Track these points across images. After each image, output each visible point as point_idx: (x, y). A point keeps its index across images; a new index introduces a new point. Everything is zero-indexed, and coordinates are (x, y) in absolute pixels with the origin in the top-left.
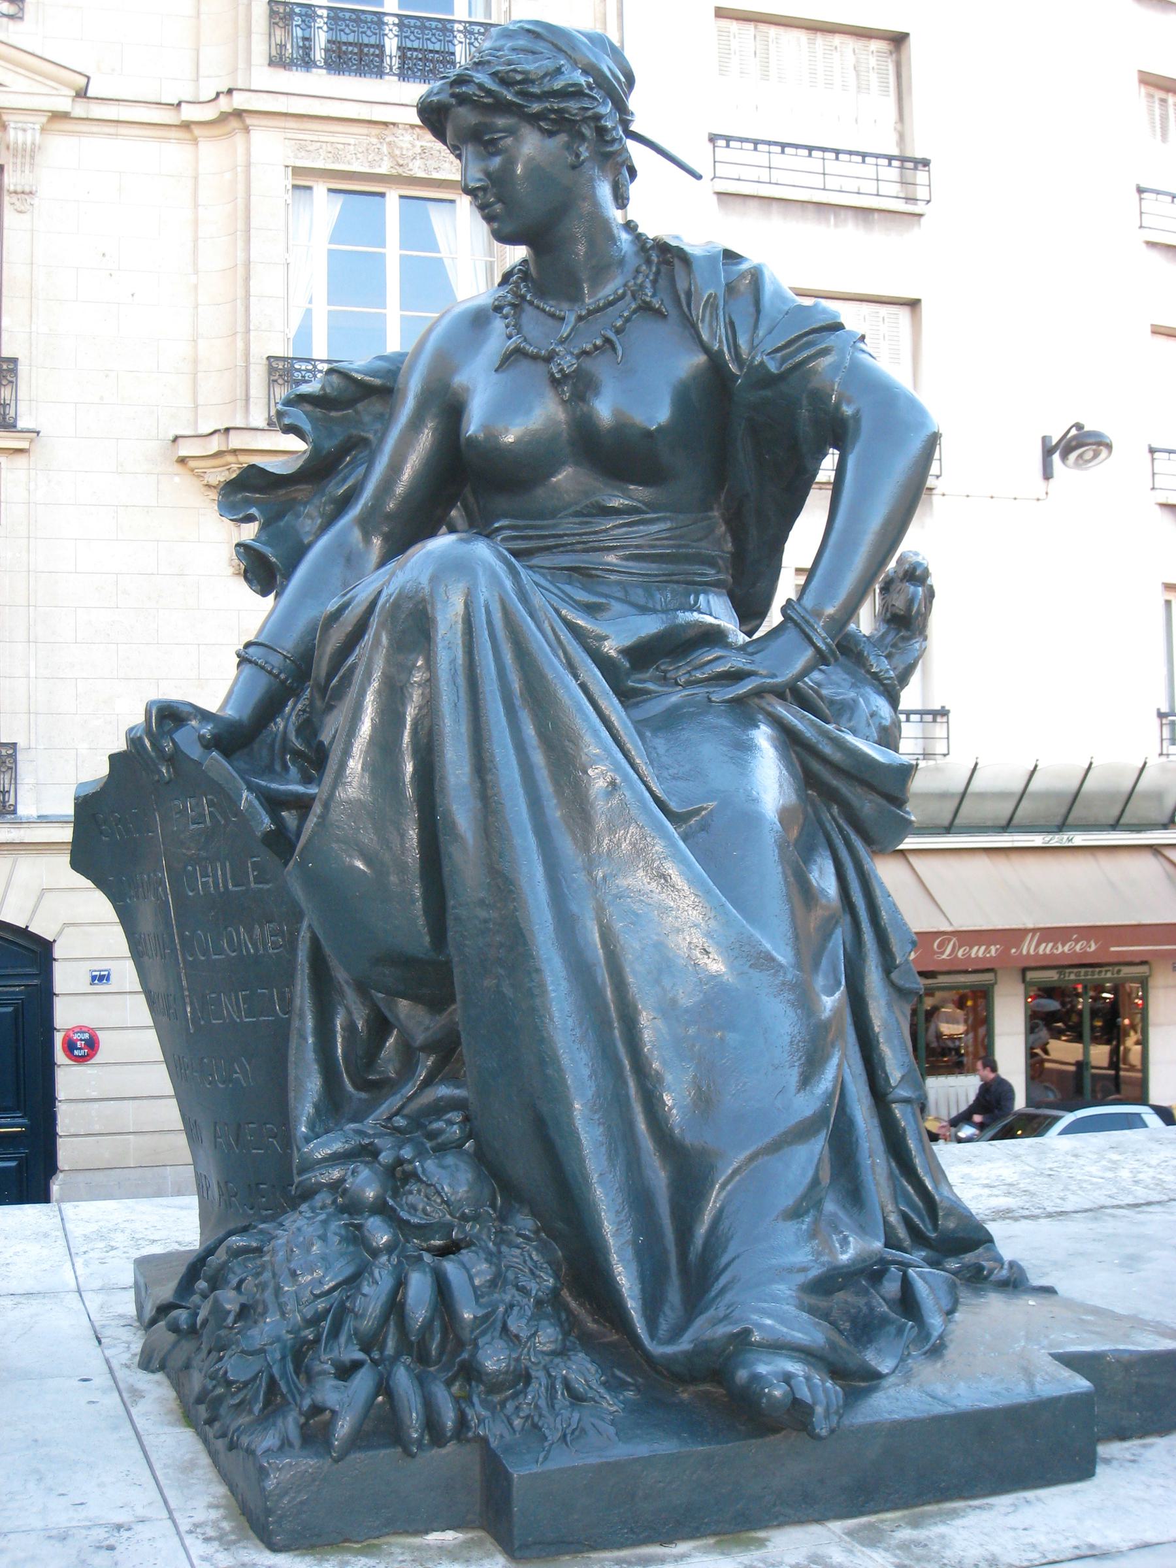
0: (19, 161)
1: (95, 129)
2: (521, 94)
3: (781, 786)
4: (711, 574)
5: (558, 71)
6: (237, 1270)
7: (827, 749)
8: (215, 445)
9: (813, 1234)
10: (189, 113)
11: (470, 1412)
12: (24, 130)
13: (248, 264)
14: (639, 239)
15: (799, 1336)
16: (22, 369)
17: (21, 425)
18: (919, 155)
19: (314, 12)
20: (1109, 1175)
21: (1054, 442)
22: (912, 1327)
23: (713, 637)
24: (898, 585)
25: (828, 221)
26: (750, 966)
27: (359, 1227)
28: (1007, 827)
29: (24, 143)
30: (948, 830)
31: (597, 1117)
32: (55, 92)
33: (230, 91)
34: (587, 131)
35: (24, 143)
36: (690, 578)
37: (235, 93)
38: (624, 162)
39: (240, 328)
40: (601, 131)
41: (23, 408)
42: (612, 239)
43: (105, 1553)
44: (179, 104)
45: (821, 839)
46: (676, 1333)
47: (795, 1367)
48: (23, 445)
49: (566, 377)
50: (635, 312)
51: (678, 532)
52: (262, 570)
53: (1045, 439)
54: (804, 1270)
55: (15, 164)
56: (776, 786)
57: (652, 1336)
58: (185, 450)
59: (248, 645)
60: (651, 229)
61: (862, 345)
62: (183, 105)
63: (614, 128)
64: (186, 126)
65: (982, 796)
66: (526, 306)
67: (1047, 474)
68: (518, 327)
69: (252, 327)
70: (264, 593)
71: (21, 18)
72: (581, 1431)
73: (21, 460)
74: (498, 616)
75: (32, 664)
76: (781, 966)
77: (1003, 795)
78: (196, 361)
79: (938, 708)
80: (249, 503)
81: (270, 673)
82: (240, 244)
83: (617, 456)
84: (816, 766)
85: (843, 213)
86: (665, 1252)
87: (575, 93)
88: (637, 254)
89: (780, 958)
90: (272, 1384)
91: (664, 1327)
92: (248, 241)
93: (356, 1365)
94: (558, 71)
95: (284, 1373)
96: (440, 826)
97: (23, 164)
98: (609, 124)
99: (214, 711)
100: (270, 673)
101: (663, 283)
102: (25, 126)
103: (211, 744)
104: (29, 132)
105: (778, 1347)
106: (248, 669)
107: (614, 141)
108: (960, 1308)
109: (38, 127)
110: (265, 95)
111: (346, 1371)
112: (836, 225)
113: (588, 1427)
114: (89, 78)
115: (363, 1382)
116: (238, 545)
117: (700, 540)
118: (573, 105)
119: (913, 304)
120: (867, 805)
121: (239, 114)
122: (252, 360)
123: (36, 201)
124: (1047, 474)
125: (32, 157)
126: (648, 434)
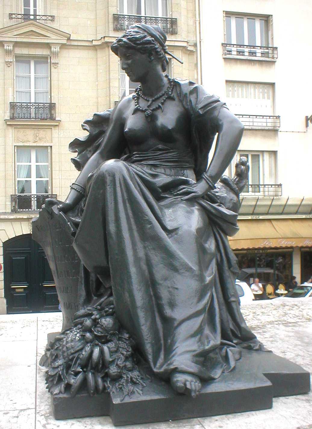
0: (55, 55)
1: (70, 47)
2: (134, 44)
3: (198, 222)
4: (188, 165)
5: (145, 37)
6: (57, 344)
7: (213, 211)
9: (200, 340)
10: (95, 43)
11: (106, 385)
12: (55, 48)
13: (109, 79)
14: (169, 79)
15: (191, 370)
16: (57, 106)
17: (57, 119)
18: (275, 46)
19: (119, 16)
20: (93, 317)
21: (309, 117)
22: (225, 365)
23: (186, 182)
24: (239, 166)
25: (251, 64)
26: (186, 271)
27: (84, 336)
28: (296, 213)
29: (56, 51)
30: (282, 214)
31: (143, 310)
32: (62, 39)
33: (104, 37)
34: (153, 53)
35: (56, 51)
36: (182, 166)
37: (105, 38)
38: (164, 60)
39: (108, 95)
40: (157, 52)
41: (57, 115)
42: (162, 80)
43: (16, 418)
44: (92, 40)
45: (212, 234)
46: (161, 366)
47: (189, 378)
48: (58, 124)
49: (149, 116)
50: (167, 98)
51: (178, 155)
52: (79, 165)
53: (307, 117)
54: (194, 351)
55: (53, 56)
56: (197, 223)
57: (155, 367)
59: (73, 184)
60: (172, 77)
61: (225, 106)
62: (93, 41)
63: (160, 51)
64: (94, 46)
65: (290, 205)
66: (140, 98)
67: (307, 126)
68: (138, 103)
69: (111, 94)
70: (79, 171)
71: (54, 20)
72: (133, 392)
73: (57, 128)
74: (122, 182)
75: (60, 175)
76: (194, 270)
77: (296, 205)
78: (98, 103)
79: (279, 184)
80: (76, 147)
81: (77, 191)
82: (108, 74)
83: (165, 137)
84: (212, 216)
85: (255, 62)
86: (161, 345)
87: (149, 42)
88: (168, 83)
89: (194, 268)
90: (60, 376)
91: (158, 365)
92: (109, 74)
93: (79, 372)
94: (145, 37)
95: (63, 373)
96: (107, 234)
97: (55, 56)
98: (159, 50)
99: (63, 201)
100: (77, 191)
101: (174, 90)
102: (56, 47)
103: (60, 210)
104: (57, 49)
105: (184, 372)
106: (73, 190)
107: (161, 54)
108: (242, 358)
109: (59, 47)
110: (113, 38)
111: (76, 374)
112: (254, 65)
113: (136, 392)
114: (70, 35)
115: (80, 376)
116: (71, 159)
117: (185, 156)
118: (149, 46)
119: (273, 85)
120: (224, 226)
122: (111, 102)
123: (59, 65)
124: (307, 126)
125: (58, 54)
126: (169, 130)
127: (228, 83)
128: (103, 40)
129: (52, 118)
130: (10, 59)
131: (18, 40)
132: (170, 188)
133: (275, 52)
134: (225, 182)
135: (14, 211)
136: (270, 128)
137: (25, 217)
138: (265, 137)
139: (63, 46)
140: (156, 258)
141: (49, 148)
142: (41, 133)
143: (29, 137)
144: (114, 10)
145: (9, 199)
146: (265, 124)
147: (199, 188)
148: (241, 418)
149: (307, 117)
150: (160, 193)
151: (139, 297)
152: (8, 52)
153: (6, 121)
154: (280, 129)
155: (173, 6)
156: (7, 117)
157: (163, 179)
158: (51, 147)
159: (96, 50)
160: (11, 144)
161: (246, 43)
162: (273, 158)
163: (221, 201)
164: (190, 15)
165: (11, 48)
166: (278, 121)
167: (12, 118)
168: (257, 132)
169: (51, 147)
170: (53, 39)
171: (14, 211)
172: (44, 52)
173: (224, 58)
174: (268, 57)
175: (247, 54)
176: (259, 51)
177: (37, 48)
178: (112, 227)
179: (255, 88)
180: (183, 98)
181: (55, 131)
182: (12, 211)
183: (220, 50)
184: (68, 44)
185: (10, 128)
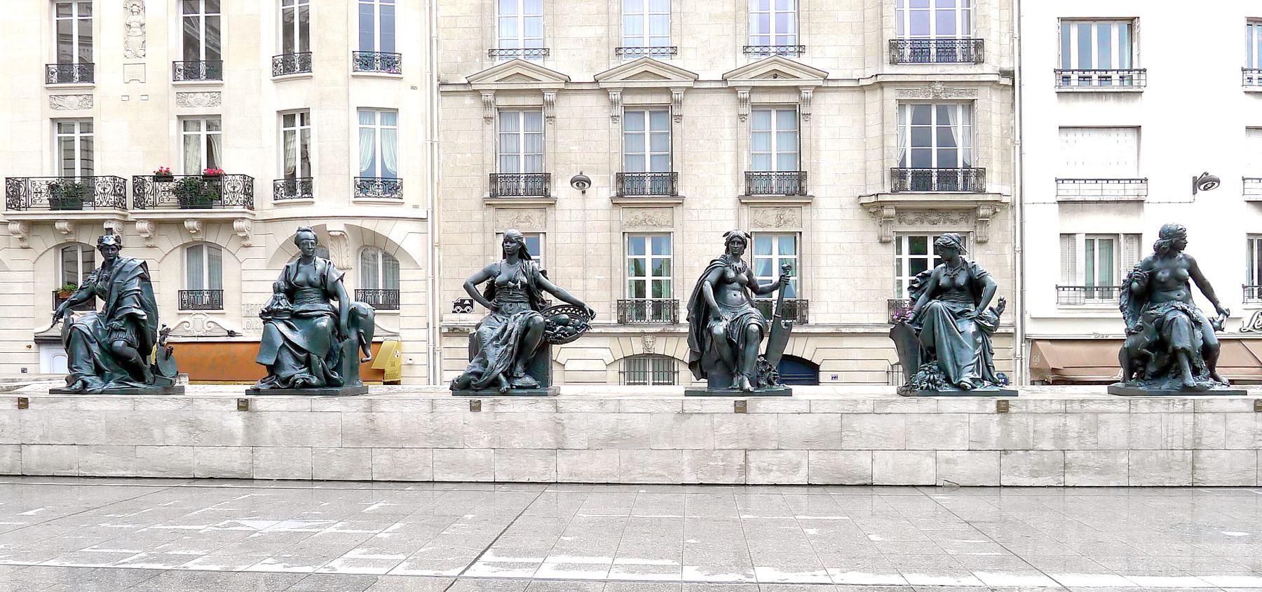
8: (873, 199)
10: (862, 83)
53: (1195, 178)
83: (960, 289)
128: (873, 80)
129: (802, 193)
130: (746, 110)
131: (628, 85)
132: (961, 314)
133: (1143, 77)
134: (991, 309)
135: (622, 322)
136: (1131, 198)
138: (1121, 212)
139: (817, 89)
140: (955, 343)
142: (788, 214)
144: (890, 34)
147: (975, 314)
149: (1195, 178)
150: (957, 316)
151: (948, 357)
152: (743, 101)
153: (740, 198)
156: (742, 192)
157: (959, 310)
161: (1095, 67)
162: (1136, 244)
163: (989, 320)
164: (1005, 29)
166: (1143, 186)
167: (748, 194)
171: (622, 322)
172: (792, 98)
174: (1128, 83)
175: (1095, 82)
176: (1115, 76)
178: (936, 330)
180: (969, 270)
181: (806, 210)
183: (1051, 80)
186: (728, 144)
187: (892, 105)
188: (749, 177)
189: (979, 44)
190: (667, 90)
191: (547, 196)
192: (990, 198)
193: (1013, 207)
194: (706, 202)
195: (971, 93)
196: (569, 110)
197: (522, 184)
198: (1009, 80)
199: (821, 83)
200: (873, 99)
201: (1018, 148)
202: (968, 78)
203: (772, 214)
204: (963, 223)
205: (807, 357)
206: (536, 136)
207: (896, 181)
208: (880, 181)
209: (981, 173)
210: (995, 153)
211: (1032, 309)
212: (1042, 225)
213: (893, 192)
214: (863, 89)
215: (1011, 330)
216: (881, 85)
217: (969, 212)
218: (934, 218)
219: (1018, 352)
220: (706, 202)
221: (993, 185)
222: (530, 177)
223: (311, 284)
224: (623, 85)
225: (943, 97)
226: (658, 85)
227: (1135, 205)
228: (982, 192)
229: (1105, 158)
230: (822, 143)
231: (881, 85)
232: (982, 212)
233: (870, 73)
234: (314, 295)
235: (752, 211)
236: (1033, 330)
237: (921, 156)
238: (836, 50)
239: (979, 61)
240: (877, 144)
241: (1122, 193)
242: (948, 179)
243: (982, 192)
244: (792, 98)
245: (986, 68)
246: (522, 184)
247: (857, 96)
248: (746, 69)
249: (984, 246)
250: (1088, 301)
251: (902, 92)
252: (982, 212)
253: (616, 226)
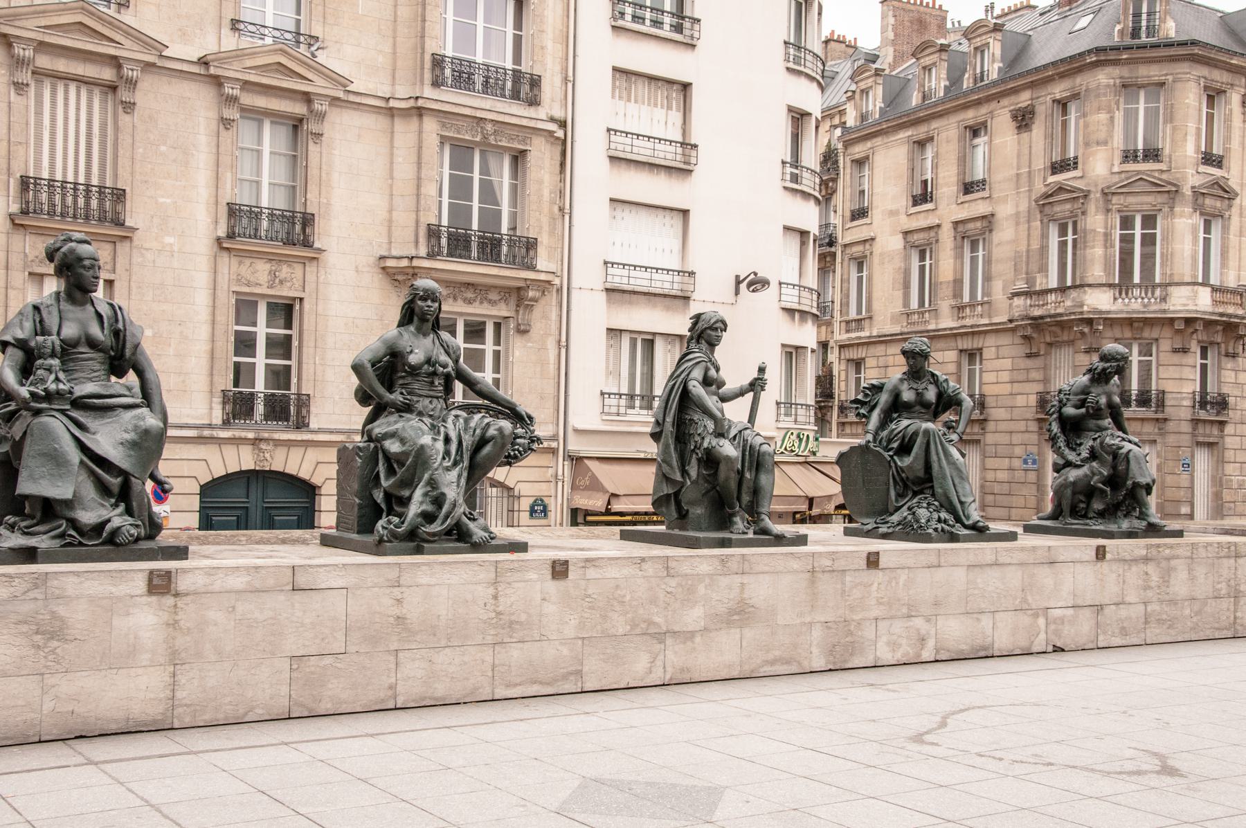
8: (405, 263)
10: (392, 104)
17: (316, 245)
33: (417, 98)
53: (737, 277)
58: (390, 263)
64: (391, 109)
67: (737, 293)
121: (419, 108)
124: (737, 293)
127: (788, 233)
128: (411, 103)
129: (307, 244)
131: (48, 39)
135: (226, 423)
137: (251, 435)
138: (668, 308)
141: (297, 302)
142: (284, 271)
143: (259, 277)
145: (217, 400)
146: (646, 283)
148: (964, 647)
149: (737, 277)
153: (219, 240)
154: (694, 296)
155: (536, 50)
156: (222, 232)
158: (301, 299)
159: (393, 116)
160: (226, 287)
165: (29, 53)
167: (231, 236)
168: (657, 299)
169: (301, 299)
170: (319, 86)
173: (611, 158)
177: (286, 98)
179: (668, 218)
181: (311, 268)
182: (223, 422)
184: (346, 100)
185: (225, 254)
186: (202, 159)
187: (431, 140)
188: (233, 211)
189: (535, 82)
190: (116, 62)
191: (119, 223)
192: (543, 277)
193: (559, 291)
194: (169, 240)
195: (524, 141)
196: (152, 95)
197: (265, 224)
198: (562, 140)
199: (341, 95)
200: (405, 132)
201: (567, 217)
202: (525, 122)
203: (262, 270)
204: (503, 305)
205: (304, 475)
206: (296, 162)
207: (433, 241)
208: (413, 238)
209: (531, 245)
210: (545, 220)
211: (576, 421)
212: (590, 315)
213: (431, 256)
214: (391, 113)
215: (554, 445)
216: (420, 112)
217: (517, 295)
218: (470, 295)
219: (560, 472)
220: (169, 240)
221: (544, 261)
222: (288, 218)
223: (92, 344)
224: (40, 37)
225: (492, 140)
226: (285, 85)
227: (679, 302)
228: (532, 268)
229: (650, 245)
230: (335, 176)
231: (420, 112)
232: (531, 294)
233: (402, 92)
234: (94, 362)
235: (234, 261)
236: (577, 446)
237: (460, 213)
238: (358, 54)
239: (534, 102)
240: (410, 189)
241: (625, 280)
242: (490, 249)
243: (532, 268)
244: (299, 109)
245: (541, 113)
246: (265, 224)
247: (381, 122)
248: (239, 54)
249: (526, 336)
250: (629, 411)
251: (444, 125)
252: (531, 294)
253: (16, 260)
